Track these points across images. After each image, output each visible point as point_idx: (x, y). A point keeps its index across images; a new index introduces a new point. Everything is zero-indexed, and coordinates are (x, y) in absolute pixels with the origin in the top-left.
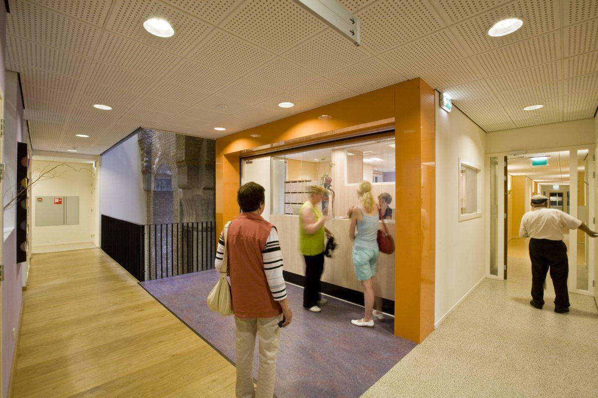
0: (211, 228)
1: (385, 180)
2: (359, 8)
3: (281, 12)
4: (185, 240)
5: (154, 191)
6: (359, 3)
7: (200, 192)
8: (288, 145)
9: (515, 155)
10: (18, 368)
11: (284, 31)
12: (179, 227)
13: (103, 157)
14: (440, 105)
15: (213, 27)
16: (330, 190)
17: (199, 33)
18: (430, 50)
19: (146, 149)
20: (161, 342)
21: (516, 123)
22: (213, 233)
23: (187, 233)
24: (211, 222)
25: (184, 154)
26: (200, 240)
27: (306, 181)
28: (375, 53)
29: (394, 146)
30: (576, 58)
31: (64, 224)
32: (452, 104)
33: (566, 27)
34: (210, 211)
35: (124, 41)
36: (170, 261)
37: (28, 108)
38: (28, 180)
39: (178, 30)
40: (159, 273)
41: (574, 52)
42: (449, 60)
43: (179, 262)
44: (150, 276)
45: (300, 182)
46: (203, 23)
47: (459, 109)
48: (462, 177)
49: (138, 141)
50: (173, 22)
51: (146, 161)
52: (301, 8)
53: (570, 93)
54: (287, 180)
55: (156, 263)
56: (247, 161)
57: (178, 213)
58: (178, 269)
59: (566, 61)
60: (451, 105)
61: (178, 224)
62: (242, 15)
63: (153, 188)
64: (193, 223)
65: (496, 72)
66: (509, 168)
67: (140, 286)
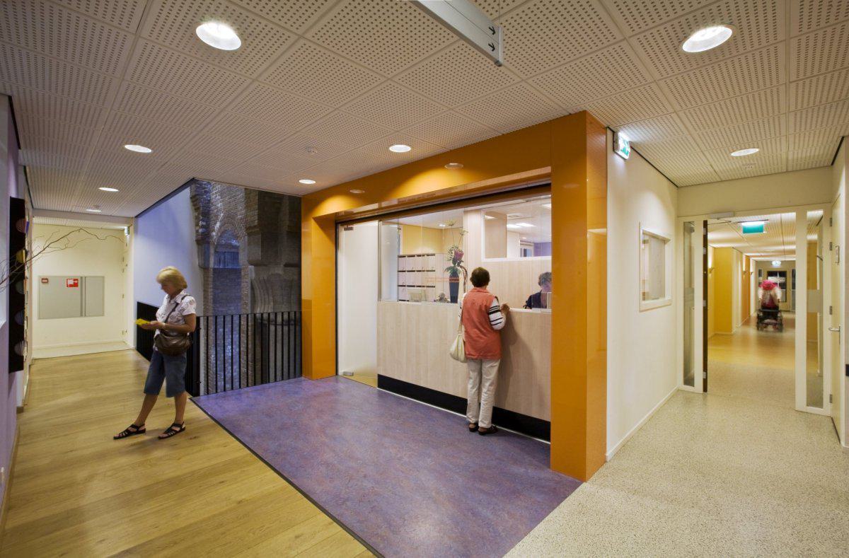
0: (295, 321)
1: (537, 253)
2: (502, 12)
3: (396, 14)
4: (258, 337)
5: (214, 269)
6: (502, 4)
7: (279, 270)
8: (402, 205)
9: (718, 219)
10: (7, 527)
11: (403, 44)
12: (250, 319)
13: (140, 220)
14: (614, 150)
15: (306, 36)
16: (461, 267)
17: (276, 45)
18: (611, 67)
19: (202, 209)
20: (223, 482)
21: (720, 174)
22: (298, 328)
23: (260, 327)
24: (295, 313)
25: (257, 218)
26: (279, 338)
27: (428, 255)
28: (524, 77)
29: (549, 206)
30: (808, 81)
31: (81, 315)
32: (631, 147)
33: (781, 41)
34: (294, 298)
35: (187, 61)
36: (236, 367)
37: (26, 148)
38: (26, 253)
39: (246, 40)
40: (221, 384)
41: (827, 68)
42: (617, 88)
43: (250, 368)
44: (208, 389)
45: (419, 256)
46: (282, 31)
47: (642, 157)
48: (643, 250)
49: (191, 198)
50: (238, 29)
51: (202, 227)
52: (421, 12)
53: (798, 131)
54: (401, 254)
55: (216, 370)
56: (346, 226)
57: (249, 301)
58: (248, 378)
59: (794, 85)
60: (629, 149)
61: (248, 315)
62: (341, 17)
63: (212, 265)
64: (269, 314)
65: (693, 103)
66: (710, 236)
67: (193, 403)
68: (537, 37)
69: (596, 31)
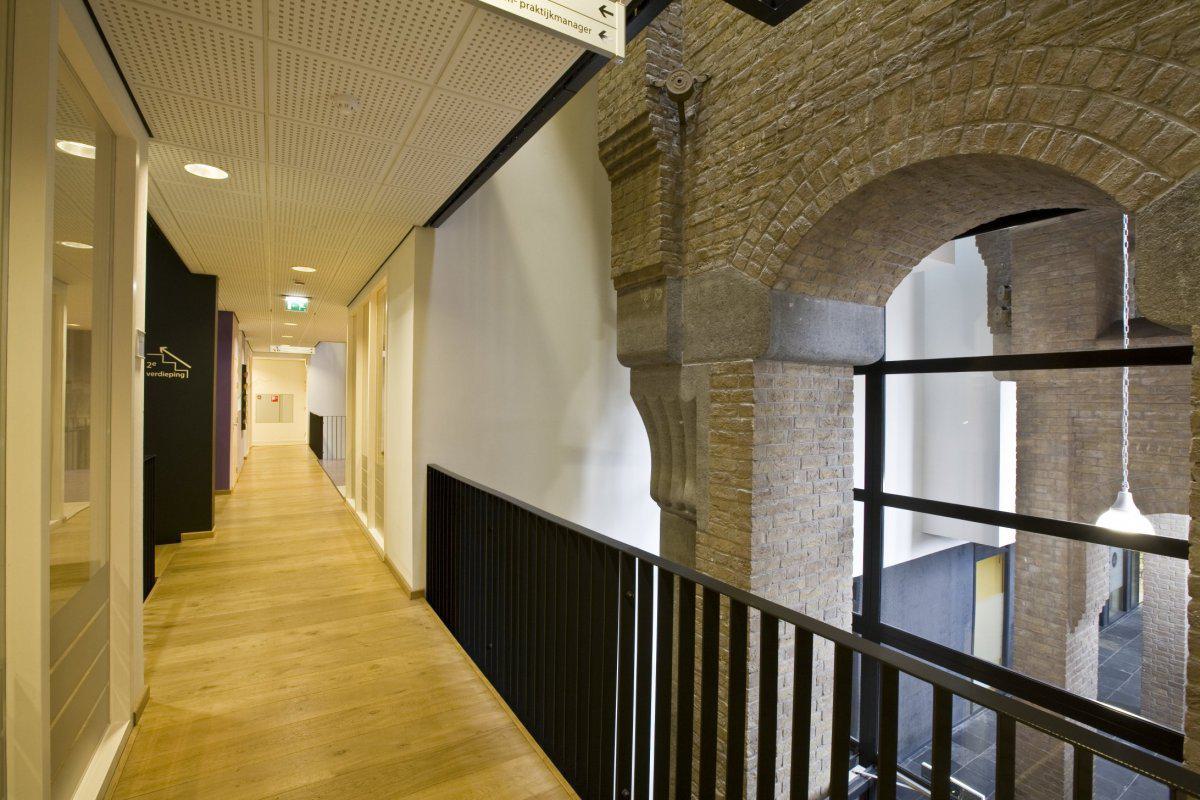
68: (492, 49)
69: (335, 30)
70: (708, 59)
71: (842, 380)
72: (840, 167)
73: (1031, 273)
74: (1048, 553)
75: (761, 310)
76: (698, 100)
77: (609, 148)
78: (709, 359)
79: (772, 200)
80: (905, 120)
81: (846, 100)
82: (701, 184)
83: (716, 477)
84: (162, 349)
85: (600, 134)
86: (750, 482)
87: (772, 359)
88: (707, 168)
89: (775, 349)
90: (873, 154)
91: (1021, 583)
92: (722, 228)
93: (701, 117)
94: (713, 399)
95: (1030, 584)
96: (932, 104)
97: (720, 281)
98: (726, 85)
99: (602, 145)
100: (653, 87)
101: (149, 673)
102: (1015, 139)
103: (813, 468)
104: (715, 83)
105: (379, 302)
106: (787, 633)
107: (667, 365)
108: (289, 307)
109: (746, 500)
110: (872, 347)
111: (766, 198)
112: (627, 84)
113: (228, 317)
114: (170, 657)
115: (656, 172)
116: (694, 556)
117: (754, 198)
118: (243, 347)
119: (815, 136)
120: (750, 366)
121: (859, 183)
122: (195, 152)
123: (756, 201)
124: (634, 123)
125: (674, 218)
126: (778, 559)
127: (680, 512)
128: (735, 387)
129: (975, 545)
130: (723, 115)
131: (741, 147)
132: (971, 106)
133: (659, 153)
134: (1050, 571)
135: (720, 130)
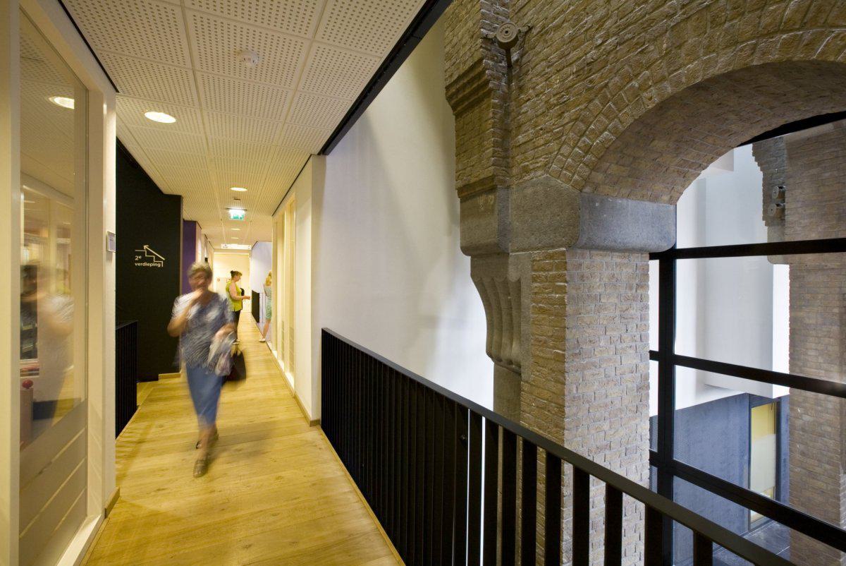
70: (529, 13)
71: (640, 264)
72: (639, 88)
73: (804, 175)
74: (821, 406)
75: (572, 209)
76: (522, 47)
77: (453, 90)
78: (531, 248)
79: (582, 121)
80: (701, 42)
81: (646, 31)
82: (523, 113)
83: (537, 340)
84: (145, 247)
85: (446, 80)
86: (564, 345)
87: (581, 248)
88: (529, 99)
89: (584, 240)
90: (670, 74)
91: (795, 429)
92: (540, 146)
93: (524, 59)
94: (534, 279)
95: (803, 430)
96: (727, 25)
97: (539, 188)
98: (544, 32)
99: (447, 88)
100: (486, 38)
101: (120, 478)
102: (811, 45)
103: (616, 334)
104: (535, 32)
105: (291, 212)
106: (597, 490)
107: (499, 254)
108: (232, 217)
109: (561, 359)
110: (665, 237)
111: (576, 119)
112: (467, 37)
113: (192, 225)
114: (139, 465)
115: (488, 106)
116: (519, 400)
117: (566, 120)
118: (206, 245)
119: (619, 65)
120: (563, 254)
121: (657, 100)
122: (164, 105)
123: (567, 123)
124: (472, 68)
125: (503, 140)
126: (587, 406)
127: (509, 366)
128: (551, 270)
129: (750, 396)
130: (541, 56)
131: (556, 80)
132: (766, 20)
133: (491, 90)
134: (822, 421)
135: (539, 68)
